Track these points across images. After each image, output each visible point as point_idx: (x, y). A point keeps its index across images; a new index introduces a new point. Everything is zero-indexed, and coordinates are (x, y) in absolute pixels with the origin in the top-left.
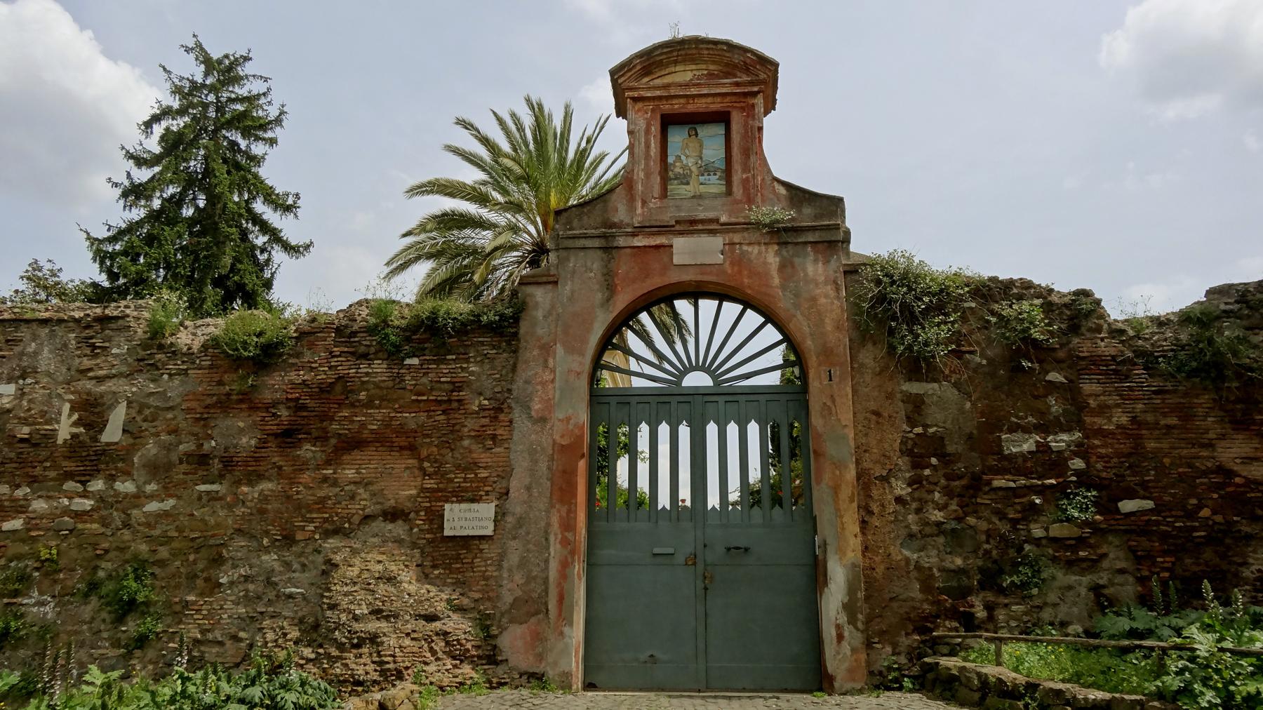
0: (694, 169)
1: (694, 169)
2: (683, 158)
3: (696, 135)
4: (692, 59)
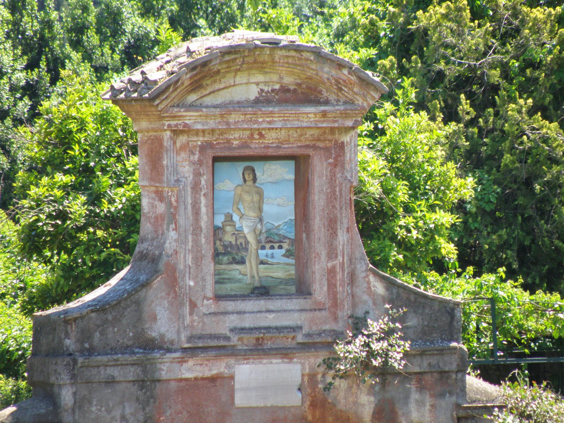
0: (251, 239)
1: (251, 239)
2: (236, 218)
3: (255, 180)
4: (260, 66)
